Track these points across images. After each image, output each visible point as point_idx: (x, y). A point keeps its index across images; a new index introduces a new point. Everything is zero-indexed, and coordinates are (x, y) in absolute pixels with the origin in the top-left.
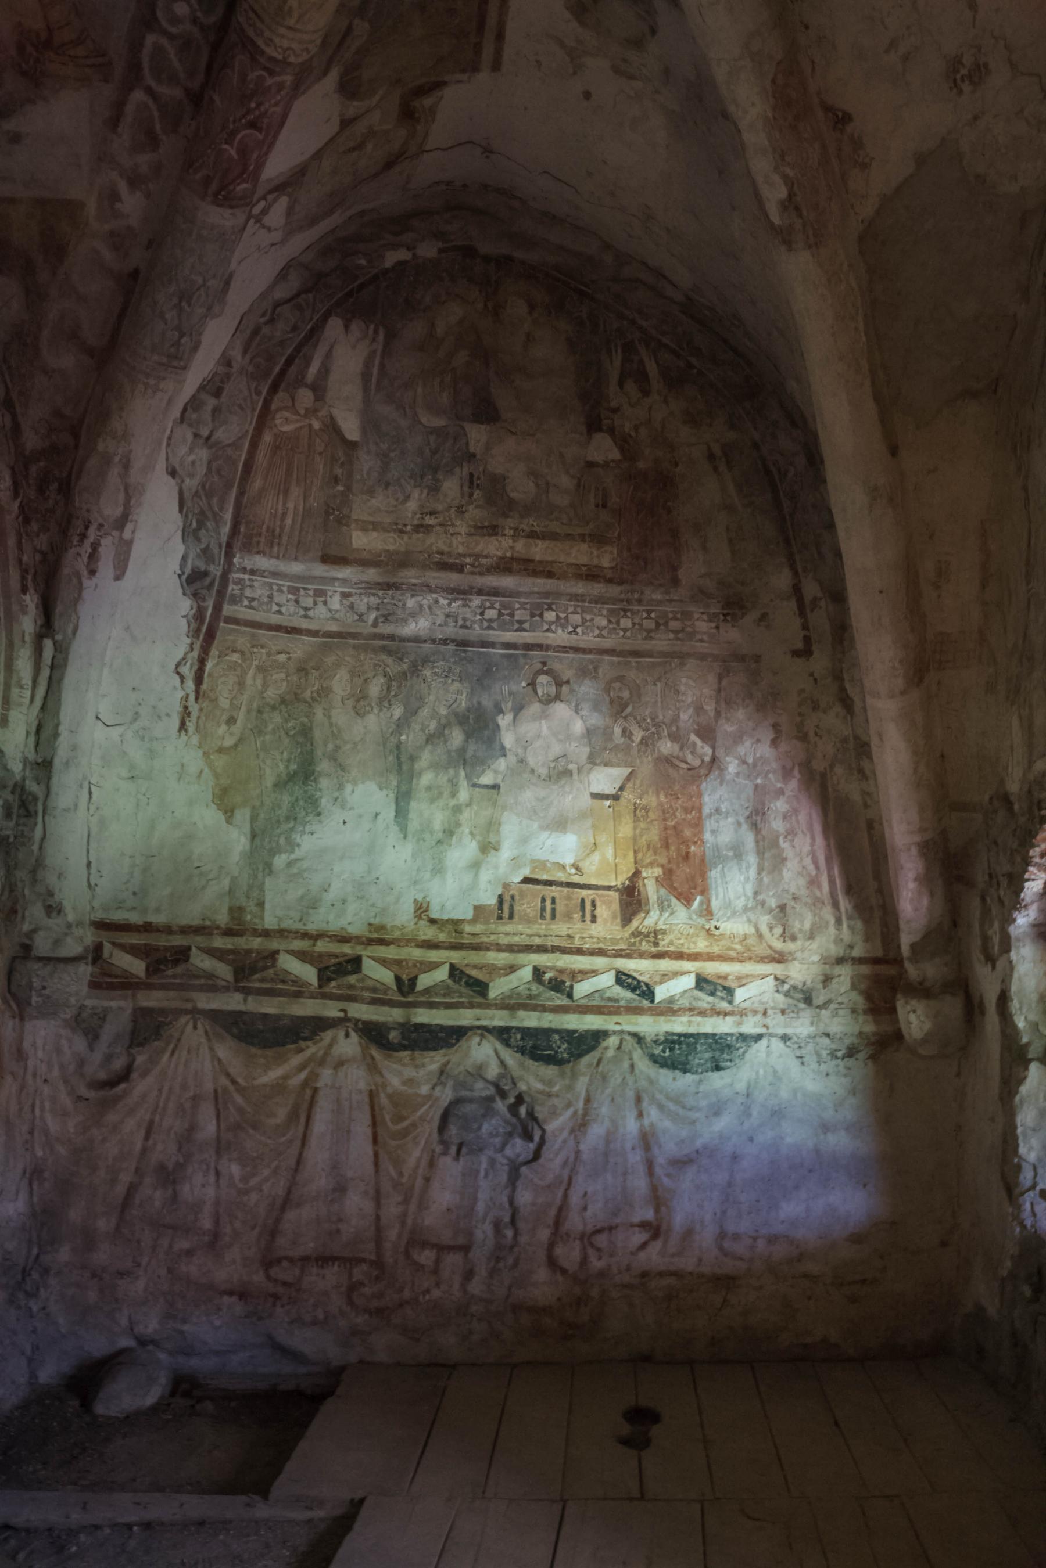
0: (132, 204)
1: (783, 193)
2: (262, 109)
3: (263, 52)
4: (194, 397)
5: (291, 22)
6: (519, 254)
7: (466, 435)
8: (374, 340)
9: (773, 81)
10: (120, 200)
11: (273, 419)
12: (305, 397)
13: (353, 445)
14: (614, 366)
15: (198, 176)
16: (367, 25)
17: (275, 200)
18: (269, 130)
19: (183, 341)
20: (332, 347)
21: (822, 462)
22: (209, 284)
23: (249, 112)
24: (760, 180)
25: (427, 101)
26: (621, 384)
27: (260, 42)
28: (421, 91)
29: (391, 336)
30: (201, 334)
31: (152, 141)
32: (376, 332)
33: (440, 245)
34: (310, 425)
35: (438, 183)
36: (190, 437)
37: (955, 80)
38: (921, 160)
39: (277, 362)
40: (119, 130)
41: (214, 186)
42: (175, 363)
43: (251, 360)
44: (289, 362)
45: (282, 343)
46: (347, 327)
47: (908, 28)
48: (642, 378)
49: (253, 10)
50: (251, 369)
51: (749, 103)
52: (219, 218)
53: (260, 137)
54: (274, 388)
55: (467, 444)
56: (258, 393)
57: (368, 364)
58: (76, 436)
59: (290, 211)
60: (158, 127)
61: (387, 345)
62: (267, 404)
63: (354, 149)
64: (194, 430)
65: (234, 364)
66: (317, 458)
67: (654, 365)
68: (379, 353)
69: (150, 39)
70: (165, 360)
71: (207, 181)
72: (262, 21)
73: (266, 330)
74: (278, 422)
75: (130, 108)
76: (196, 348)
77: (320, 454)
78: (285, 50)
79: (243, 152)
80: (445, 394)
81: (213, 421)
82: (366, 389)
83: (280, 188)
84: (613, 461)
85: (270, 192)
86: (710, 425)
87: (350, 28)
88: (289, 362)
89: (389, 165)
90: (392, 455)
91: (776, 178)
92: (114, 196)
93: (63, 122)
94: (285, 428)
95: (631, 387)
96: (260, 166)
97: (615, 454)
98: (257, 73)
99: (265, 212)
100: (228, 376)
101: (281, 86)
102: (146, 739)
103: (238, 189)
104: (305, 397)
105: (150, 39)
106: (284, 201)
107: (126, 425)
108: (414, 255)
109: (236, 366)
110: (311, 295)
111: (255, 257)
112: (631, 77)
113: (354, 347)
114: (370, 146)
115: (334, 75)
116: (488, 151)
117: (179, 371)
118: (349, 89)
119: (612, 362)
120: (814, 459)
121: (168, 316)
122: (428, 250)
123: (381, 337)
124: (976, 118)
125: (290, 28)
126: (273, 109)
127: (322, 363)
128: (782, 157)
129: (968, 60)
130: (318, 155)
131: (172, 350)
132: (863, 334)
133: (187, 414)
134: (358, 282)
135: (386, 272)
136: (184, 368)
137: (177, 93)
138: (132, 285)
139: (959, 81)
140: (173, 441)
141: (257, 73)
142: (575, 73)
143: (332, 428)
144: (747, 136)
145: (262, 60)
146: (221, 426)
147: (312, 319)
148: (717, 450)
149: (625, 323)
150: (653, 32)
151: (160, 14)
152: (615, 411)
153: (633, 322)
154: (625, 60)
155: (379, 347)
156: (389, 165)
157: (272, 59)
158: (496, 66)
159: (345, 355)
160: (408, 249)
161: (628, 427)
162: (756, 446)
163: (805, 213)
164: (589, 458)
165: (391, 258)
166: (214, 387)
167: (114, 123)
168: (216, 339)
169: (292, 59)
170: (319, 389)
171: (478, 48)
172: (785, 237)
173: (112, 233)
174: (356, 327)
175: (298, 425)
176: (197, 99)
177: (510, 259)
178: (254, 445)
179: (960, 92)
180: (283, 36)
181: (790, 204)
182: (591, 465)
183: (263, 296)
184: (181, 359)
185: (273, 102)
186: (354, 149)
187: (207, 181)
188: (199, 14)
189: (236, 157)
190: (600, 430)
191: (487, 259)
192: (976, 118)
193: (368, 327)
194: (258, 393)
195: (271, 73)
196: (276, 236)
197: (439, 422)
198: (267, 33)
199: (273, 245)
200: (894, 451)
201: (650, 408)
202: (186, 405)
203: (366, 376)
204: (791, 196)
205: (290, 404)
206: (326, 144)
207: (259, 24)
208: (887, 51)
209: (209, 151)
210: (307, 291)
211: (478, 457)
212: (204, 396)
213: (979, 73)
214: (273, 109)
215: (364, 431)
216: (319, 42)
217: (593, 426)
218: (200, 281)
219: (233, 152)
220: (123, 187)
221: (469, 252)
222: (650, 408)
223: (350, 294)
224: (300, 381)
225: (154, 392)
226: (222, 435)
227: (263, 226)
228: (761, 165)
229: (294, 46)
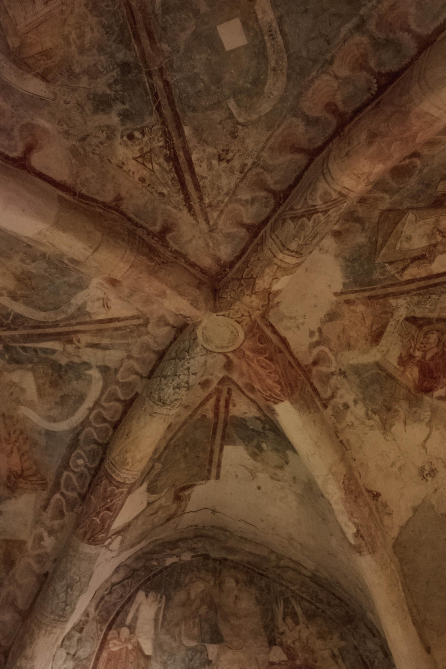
0: (49, 542)
1: (355, 530)
2: (113, 502)
3: (115, 479)
4: (69, 633)
5: (128, 467)
6: (230, 557)
7: (206, 650)
8: (160, 602)
9: (343, 483)
10: (43, 540)
11: (108, 644)
12: (125, 632)
13: (148, 658)
14: (280, 609)
15: (81, 531)
16: (160, 465)
17: (115, 538)
18: (114, 511)
19: (67, 608)
20: (139, 606)
21: (391, 655)
22: (82, 580)
23: (107, 503)
24: (343, 525)
25: (187, 493)
26: (284, 619)
27: (114, 475)
28: (184, 489)
29: (169, 599)
30: (75, 605)
31: (62, 514)
32: (161, 597)
33: (192, 554)
34: (127, 647)
35: (191, 526)
36: (65, 655)
37: (423, 476)
38: (415, 510)
39: (113, 614)
40: (47, 510)
41: (88, 536)
42: (62, 619)
43: (99, 612)
44: (118, 614)
45: (115, 605)
46: (147, 596)
47: (399, 457)
48: (294, 615)
49: (111, 463)
50: (98, 618)
51: (334, 493)
52: (88, 549)
53: (111, 514)
54: (110, 628)
55: (207, 655)
56: (101, 630)
57: (157, 614)
58: (6, 657)
59: (122, 542)
60: (64, 509)
61: (166, 605)
62: (106, 635)
63: (153, 514)
64: (67, 651)
65: (90, 615)
66: (130, 665)
67: (300, 609)
68: (163, 608)
69: (65, 474)
70: (57, 618)
71: (85, 533)
72: (115, 467)
73: (107, 598)
74: (110, 645)
75: (53, 501)
76: (72, 612)
77: (131, 663)
78: (125, 478)
79: (103, 520)
80: (196, 629)
81: (77, 645)
82: (156, 627)
83: (117, 533)
84: (283, 661)
85: (114, 535)
86: (331, 639)
87: (153, 467)
88: (118, 614)
89: (168, 520)
90: (169, 662)
91: (350, 524)
92: (41, 538)
93: (24, 505)
94: (114, 649)
95: (289, 620)
96: (110, 526)
97: (284, 657)
98: (112, 488)
99: (110, 544)
100: (87, 622)
101: (122, 493)
102: (137, 134)
103: (100, 536)
104: (125, 632)
105: (65, 474)
106: (119, 538)
107: (33, 652)
108: (180, 559)
109: (91, 616)
110: (130, 581)
111: (103, 564)
112: (279, 480)
113: (150, 606)
114: (160, 513)
115: (145, 486)
116: (214, 511)
117: (63, 623)
118: (151, 490)
119: (278, 608)
120: (387, 654)
121: (61, 596)
122: (187, 557)
123: (164, 600)
124: (436, 490)
125: (127, 470)
126: (118, 502)
127: (135, 614)
128: (352, 515)
129: (427, 468)
130: (137, 518)
131: (61, 613)
132: (402, 592)
133: (64, 643)
134: (153, 573)
135: (166, 568)
136: (66, 622)
137: (75, 495)
138: (44, 580)
139: (425, 476)
140: (56, 657)
141: (112, 488)
142: (253, 479)
143: (139, 649)
144: (334, 507)
145: (114, 483)
146: (81, 648)
147: (130, 591)
148: (336, 652)
149: (284, 588)
150: (287, 463)
151: (71, 464)
152: (282, 634)
153: (287, 588)
154: (275, 474)
155: (163, 605)
156: (168, 520)
157: (118, 482)
158: (218, 477)
159: (146, 609)
160: (177, 557)
161: (289, 642)
162: (356, 648)
163: (366, 538)
164: (271, 660)
165: (169, 561)
166: (79, 628)
167: (45, 507)
168: (83, 603)
169: (127, 482)
170: (132, 628)
171: (209, 471)
172: (358, 550)
173: (38, 555)
174: (152, 595)
175: (121, 647)
176: (83, 497)
177: (226, 559)
178: (97, 659)
179: (427, 480)
180: (124, 473)
181: (358, 534)
182: (272, 664)
183: (106, 581)
184: (65, 617)
185: (118, 499)
186: (153, 514)
187: (85, 533)
188: (88, 464)
189: (99, 522)
190: (275, 645)
191: (215, 560)
192: (436, 490)
193: (157, 595)
194: (101, 630)
195: (118, 487)
196: (114, 554)
197: (192, 644)
198: (117, 472)
199: (113, 557)
200: (428, 650)
201: (300, 631)
202: (65, 637)
203: (156, 620)
204: (358, 531)
205: (117, 636)
206: (141, 513)
207: (114, 468)
208: (391, 466)
209: (87, 520)
210: (129, 578)
211: (213, 662)
212: (73, 632)
213: (433, 472)
214: (118, 502)
215: (154, 648)
216: (140, 474)
217: (272, 642)
218: (78, 579)
219: (98, 521)
220: (45, 535)
221: (206, 557)
222: (300, 631)
223: (149, 579)
224: (122, 624)
225: (50, 634)
226: (82, 653)
227: (109, 550)
228: (343, 518)
229: (129, 477)
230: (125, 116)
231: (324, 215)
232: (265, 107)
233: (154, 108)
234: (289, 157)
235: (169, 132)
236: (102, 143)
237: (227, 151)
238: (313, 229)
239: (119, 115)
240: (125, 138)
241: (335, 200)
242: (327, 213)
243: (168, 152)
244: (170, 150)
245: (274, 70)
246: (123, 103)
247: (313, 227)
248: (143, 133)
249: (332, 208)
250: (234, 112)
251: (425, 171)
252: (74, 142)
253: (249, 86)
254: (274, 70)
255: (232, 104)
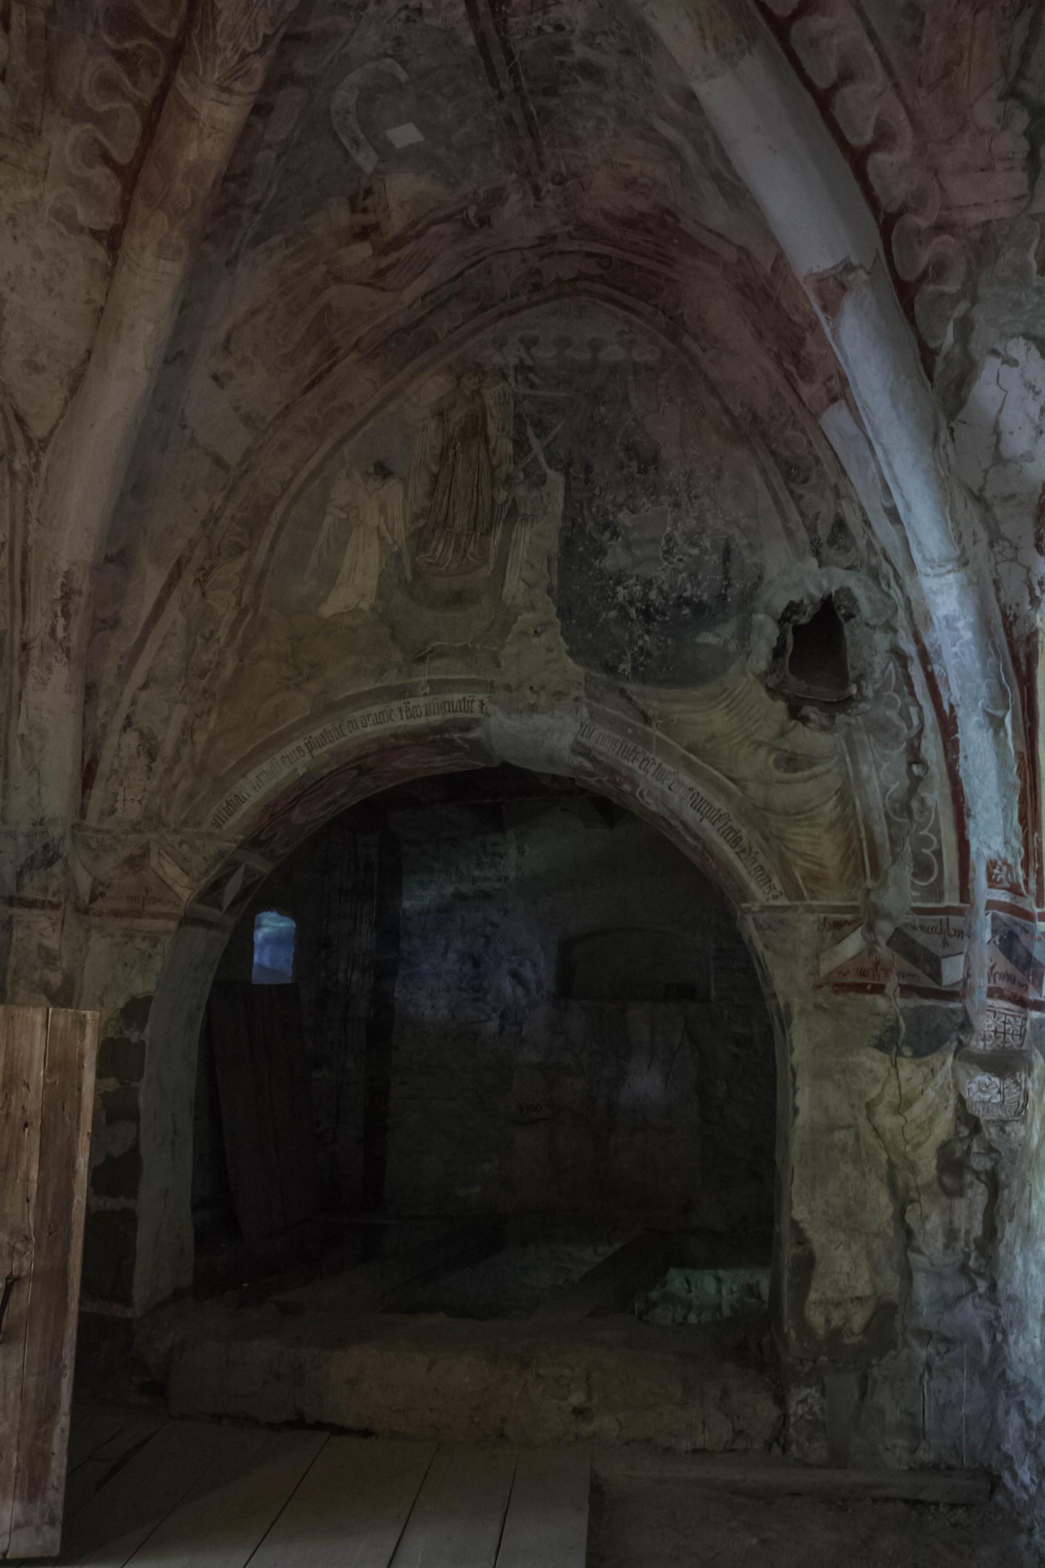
102: (549, 29)
230: (564, 48)
231: (244, 50)
232: (355, 77)
233: (517, 57)
234: (310, 27)
235: (498, 32)
236: (605, 33)
237: (408, 19)
238: (255, 20)
239: (572, 52)
240: (568, 28)
241: (236, 80)
242: (241, 56)
243: (503, 8)
244: (500, 10)
245: (348, 112)
246: (562, 63)
247: (256, 24)
248: (539, 30)
249: (235, 66)
250: (399, 68)
251: (90, 28)
252: (642, 55)
253: (380, 96)
254: (348, 112)
255: (403, 76)
